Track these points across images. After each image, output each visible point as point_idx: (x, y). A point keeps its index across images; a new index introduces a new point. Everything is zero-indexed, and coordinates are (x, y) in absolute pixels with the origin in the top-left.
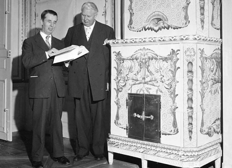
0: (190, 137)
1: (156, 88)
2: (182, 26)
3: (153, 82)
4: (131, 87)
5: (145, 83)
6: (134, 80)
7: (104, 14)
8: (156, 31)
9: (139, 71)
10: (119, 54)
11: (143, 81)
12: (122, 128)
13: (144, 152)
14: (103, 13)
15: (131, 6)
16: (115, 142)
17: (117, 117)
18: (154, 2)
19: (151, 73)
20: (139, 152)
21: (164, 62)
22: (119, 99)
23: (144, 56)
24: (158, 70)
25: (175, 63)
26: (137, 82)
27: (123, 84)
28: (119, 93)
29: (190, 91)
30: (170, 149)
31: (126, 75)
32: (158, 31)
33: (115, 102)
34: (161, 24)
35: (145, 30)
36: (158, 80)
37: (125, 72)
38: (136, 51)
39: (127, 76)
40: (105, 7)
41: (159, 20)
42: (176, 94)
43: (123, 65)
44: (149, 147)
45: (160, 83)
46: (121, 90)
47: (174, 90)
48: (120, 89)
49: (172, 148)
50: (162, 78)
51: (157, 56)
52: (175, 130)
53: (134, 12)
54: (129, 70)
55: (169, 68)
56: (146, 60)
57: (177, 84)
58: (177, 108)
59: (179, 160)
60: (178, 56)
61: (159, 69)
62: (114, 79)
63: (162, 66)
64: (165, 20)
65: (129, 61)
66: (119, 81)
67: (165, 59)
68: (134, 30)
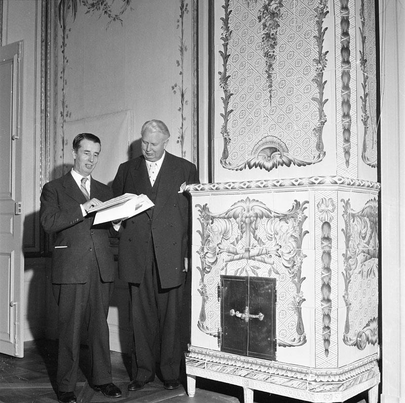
0: (327, 350)
1: (269, 267)
2: (313, 161)
3: (263, 256)
4: (226, 265)
5: (250, 258)
6: (231, 253)
7: (179, 140)
8: (268, 170)
9: (239, 237)
10: (205, 208)
11: (247, 255)
12: (211, 335)
13: (248, 376)
14: (179, 138)
15: (225, 127)
16: (198, 358)
17: (203, 317)
18: (265, 120)
19: (259, 240)
20: (240, 376)
21: (283, 223)
22: (205, 286)
23: (248, 211)
24: (272, 235)
25: (301, 223)
26: (237, 257)
27: (212, 260)
28: (206, 275)
29: (326, 271)
30: (291, 371)
31: (218, 245)
32: (271, 169)
33: (198, 290)
34: (277, 157)
35: (250, 167)
36: (272, 253)
37: (215, 239)
38: (235, 204)
39: (220, 246)
40: (182, 128)
41: (274, 150)
42: (302, 277)
43: (211, 227)
44: (257, 367)
45: (275, 258)
46: (208, 270)
47: (300, 270)
48: (206, 269)
49: (295, 368)
50: (278, 250)
51: (270, 211)
52: (300, 338)
53: (231, 137)
54: (222, 236)
55: (291, 232)
56: (252, 218)
57: (304, 260)
58: (304, 300)
59: (308, 389)
60: (306, 212)
61: (273, 233)
62: (197, 252)
63: (278, 230)
64: (284, 151)
65: (222, 221)
66: (205, 255)
67: (284, 218)
68: (230, 167)
